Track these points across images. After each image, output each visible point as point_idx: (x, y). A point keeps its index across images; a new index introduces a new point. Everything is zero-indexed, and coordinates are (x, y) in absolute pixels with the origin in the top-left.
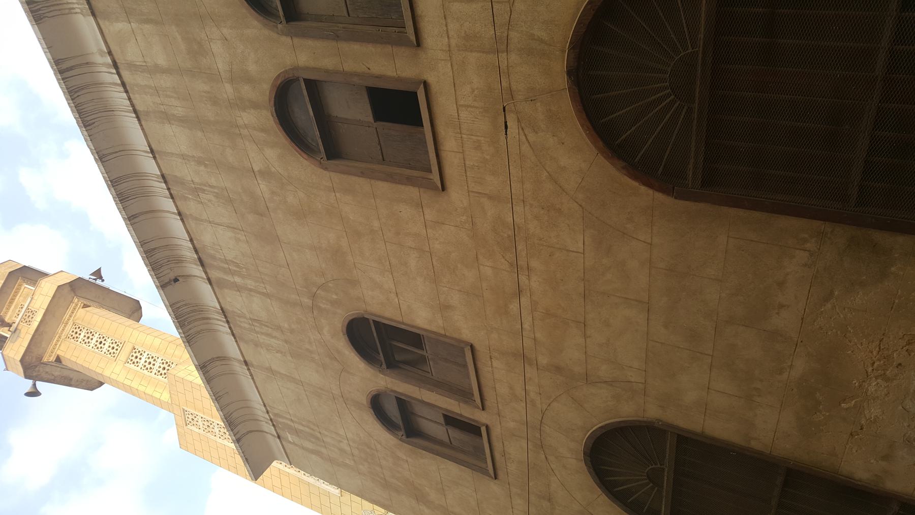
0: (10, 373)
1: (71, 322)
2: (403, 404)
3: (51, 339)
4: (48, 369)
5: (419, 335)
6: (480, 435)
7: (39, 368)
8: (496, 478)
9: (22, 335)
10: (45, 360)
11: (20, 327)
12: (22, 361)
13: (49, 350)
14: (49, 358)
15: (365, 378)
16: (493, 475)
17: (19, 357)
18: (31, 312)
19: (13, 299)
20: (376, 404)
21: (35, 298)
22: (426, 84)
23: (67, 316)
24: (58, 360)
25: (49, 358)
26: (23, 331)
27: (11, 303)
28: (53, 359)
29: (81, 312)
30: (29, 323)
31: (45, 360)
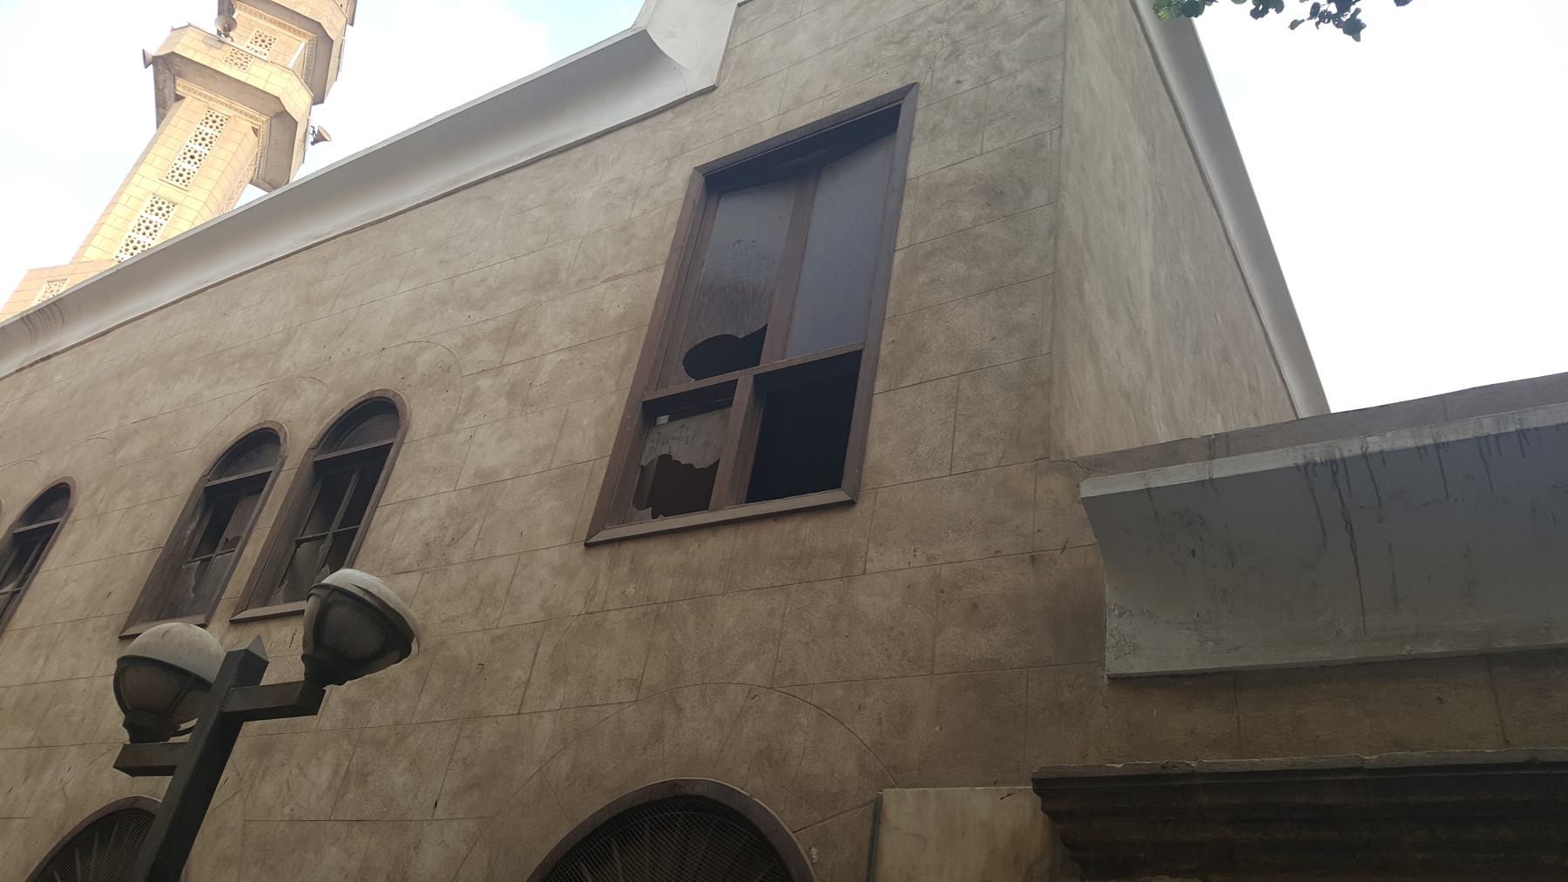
0: (167, 33)
1: (231, 113)
2: (257, 485)
3: (207, 88)
4: (169, 83)
5: (730, 404)
6: (752, 498)
7: (169, 70)
8: (588, 546)
9: (212, 52)
10: (179, 81)
11: (225, 47)
12: (173, 53)
13: (192, 86)
14: (181, 86)
15: (304, 420)
16: (593, 540)
17: (179, 50)
18: (244, 59)
19: (284, 27)
20: (262, 440)
21: (268, 67)
22: (850, 504)
23: (240, 107)
24: (179, 98)
25: (181, 86)
26: (218, 53)
27: (280, 24)
28: (180, 91)
29: (246, 125)
30: (229, 61)
31: (179, 81)
